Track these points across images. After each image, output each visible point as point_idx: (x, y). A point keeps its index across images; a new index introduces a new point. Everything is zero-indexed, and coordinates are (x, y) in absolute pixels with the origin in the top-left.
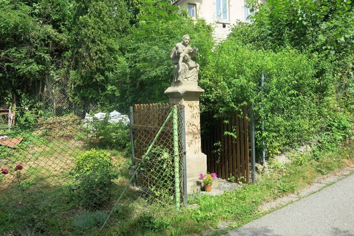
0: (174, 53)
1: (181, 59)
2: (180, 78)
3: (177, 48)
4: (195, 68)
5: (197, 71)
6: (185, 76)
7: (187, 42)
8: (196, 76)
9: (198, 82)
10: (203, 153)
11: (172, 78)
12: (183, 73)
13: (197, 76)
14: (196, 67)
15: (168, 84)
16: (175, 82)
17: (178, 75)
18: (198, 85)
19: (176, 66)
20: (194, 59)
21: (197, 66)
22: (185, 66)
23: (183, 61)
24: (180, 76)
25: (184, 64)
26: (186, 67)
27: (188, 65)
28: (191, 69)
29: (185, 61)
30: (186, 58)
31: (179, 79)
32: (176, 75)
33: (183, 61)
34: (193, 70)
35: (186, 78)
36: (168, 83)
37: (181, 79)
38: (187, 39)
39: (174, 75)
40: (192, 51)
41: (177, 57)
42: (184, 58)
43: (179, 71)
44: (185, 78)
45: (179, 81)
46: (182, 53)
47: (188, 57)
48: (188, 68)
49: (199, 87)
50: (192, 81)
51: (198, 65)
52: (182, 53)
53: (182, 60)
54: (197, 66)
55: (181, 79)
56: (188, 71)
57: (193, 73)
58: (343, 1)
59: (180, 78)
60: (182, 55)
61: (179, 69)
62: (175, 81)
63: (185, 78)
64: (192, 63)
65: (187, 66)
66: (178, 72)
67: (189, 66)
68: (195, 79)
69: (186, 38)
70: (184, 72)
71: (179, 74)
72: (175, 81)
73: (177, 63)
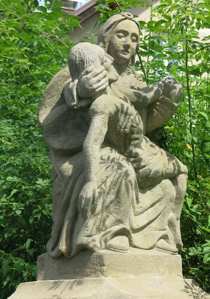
0: (56, 99)
1: (99, 127)
2: (91, 234)
3: (77, 68)
4: (167, 182)
5: (178, 199)
6: (119, 221)
7: (127, 47)
8: (171, 224)
9: (183, 255)
10: (148, 192)
11: (42, 232)
12: (106, 208)
13: (178, 224)
14: (173, 178)
15: (19, 262)
16: (61, 256)
17: (78, 213)
18: (186, 273)
19: (67, 167)
20: (159, 138)
21: (180, 172)
22: (120, 166)
23: (108, 142)
24: (91, 223)
25: (115, 154)
26: (127, 174)
27: (135, 160)
28: (147, 182)
29: (119, 139)
30: (124, 123)
31: (82, 239)
32: (70, 213)
33: (108, 142)
34: (157, 189)
35: (123, 232)
36: (21, 253)
37: (97, 237)
38: (126, 33)
39: (56, 219)
40: (150, 95)
41: (76, 115)
42: (113, 121)
43: (90, 190)
44: (117, 234)
45: (85, 250)
46: (103, 91)
47: (135, 118)
48: (133, 176)
49: (190, 281)
50: (154, 252)
51: (184, 168)
52: (103, 91)
53: (105, 130)
54: (180, 172)
55: (97, 237)
56: (133, 193)
57: (159, 207)
58: (36, 4)
59: (91, 234)
60: (105, 104)
61: (86, 180)
62: (63, 247)
63: (117, 234)
64: (154, 158)
65: (129, 167)
66: (78, 200)
67: (137, 170)
68: (165, 237)
69: (121, 26)
70: (112, 197)
71: (85, 212)
72: (63, 247)
73: (76, 152)
